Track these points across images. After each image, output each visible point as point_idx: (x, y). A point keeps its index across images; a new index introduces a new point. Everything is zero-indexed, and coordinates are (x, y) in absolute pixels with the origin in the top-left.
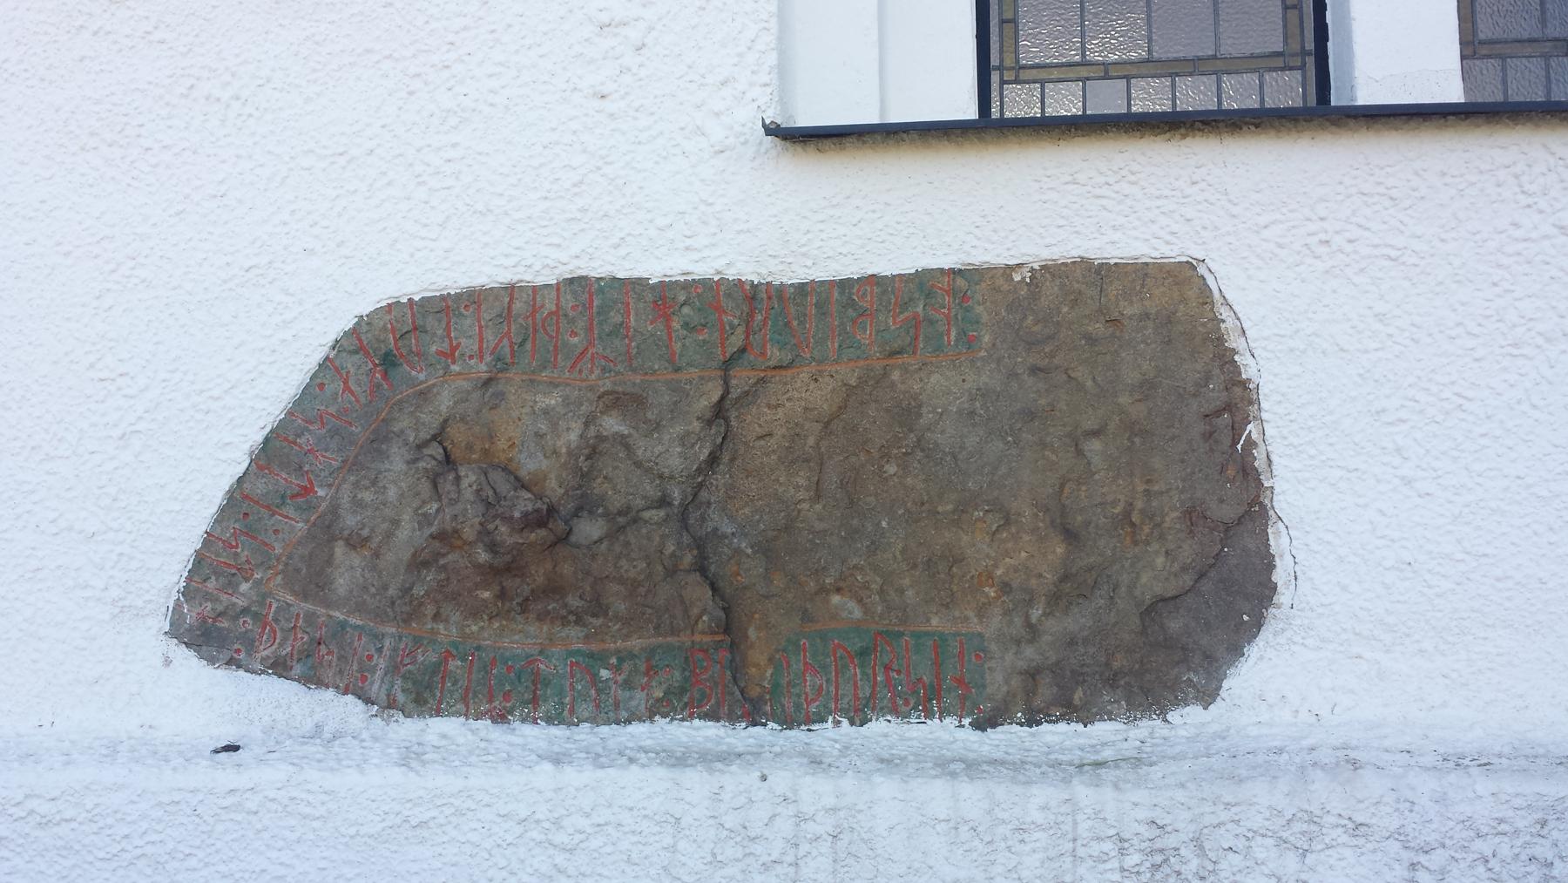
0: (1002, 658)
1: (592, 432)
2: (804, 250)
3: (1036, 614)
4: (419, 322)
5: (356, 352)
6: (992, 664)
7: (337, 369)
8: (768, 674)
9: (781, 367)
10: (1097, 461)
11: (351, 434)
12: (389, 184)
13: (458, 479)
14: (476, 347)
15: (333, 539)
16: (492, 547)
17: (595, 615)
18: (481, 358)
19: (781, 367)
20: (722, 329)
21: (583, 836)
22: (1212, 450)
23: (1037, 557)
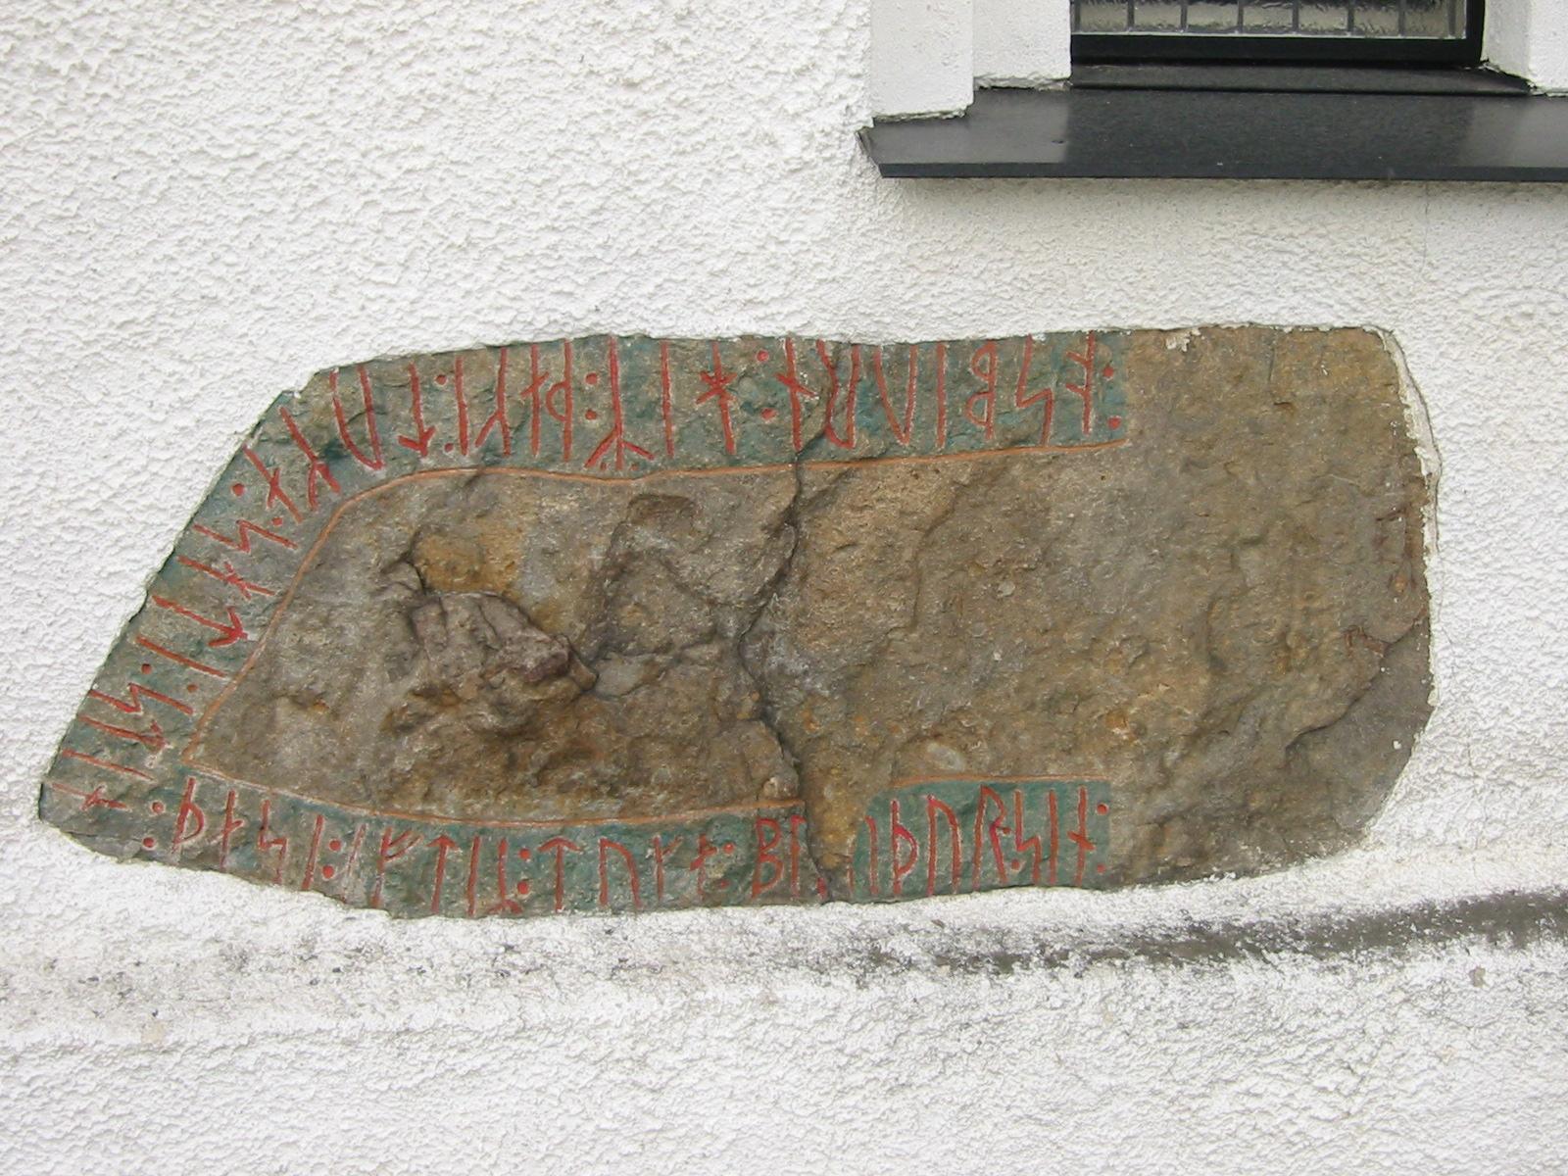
0: (1130, 809)
1: (622, 547)
2: (907, 308)
3: (1172, 756)
4: (376, 400)
5: (285, 442)
6: (1118, 816)
7: (259, 465)
8: (849, 842)
9: (871, 458)
10: (1253, 576)
11: (290, 555)
12: (324, 202)
13: (444, 614)
14: (455, 435)
15: (274, 696)
16: (500, 707)
17: (635, 784)
18: (464, 446)
19: (871, 458)
20: (796, 410)
21: (673, 1073)
22: (1381, 559)
23: (1178, 694)
